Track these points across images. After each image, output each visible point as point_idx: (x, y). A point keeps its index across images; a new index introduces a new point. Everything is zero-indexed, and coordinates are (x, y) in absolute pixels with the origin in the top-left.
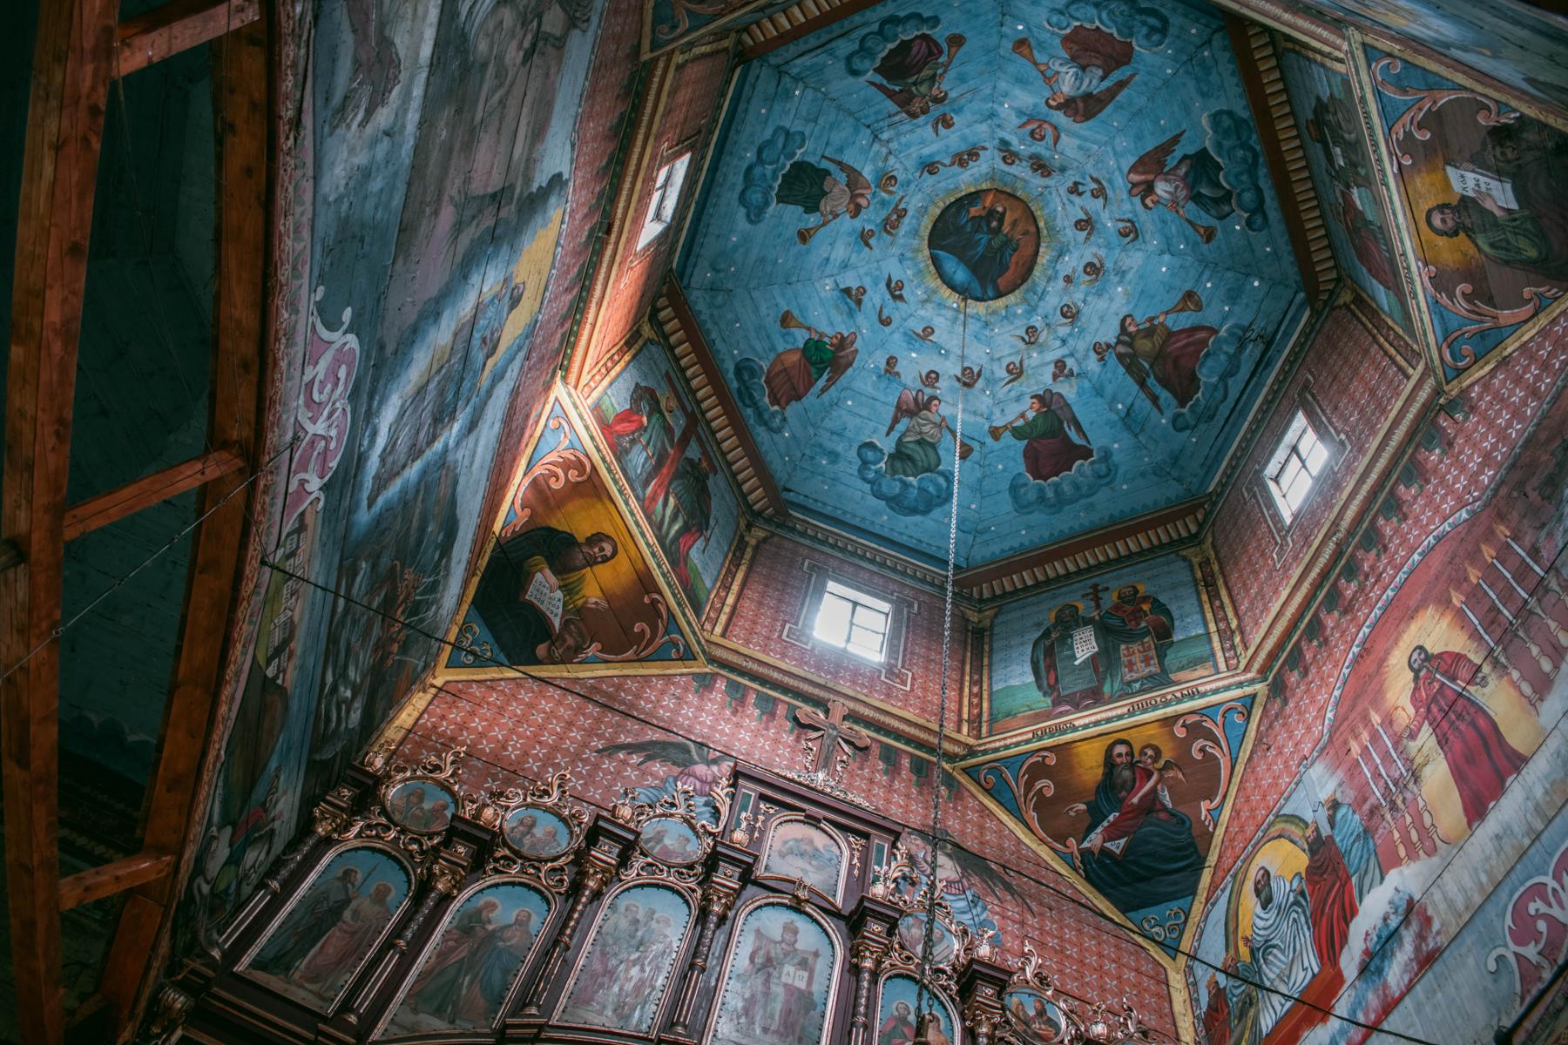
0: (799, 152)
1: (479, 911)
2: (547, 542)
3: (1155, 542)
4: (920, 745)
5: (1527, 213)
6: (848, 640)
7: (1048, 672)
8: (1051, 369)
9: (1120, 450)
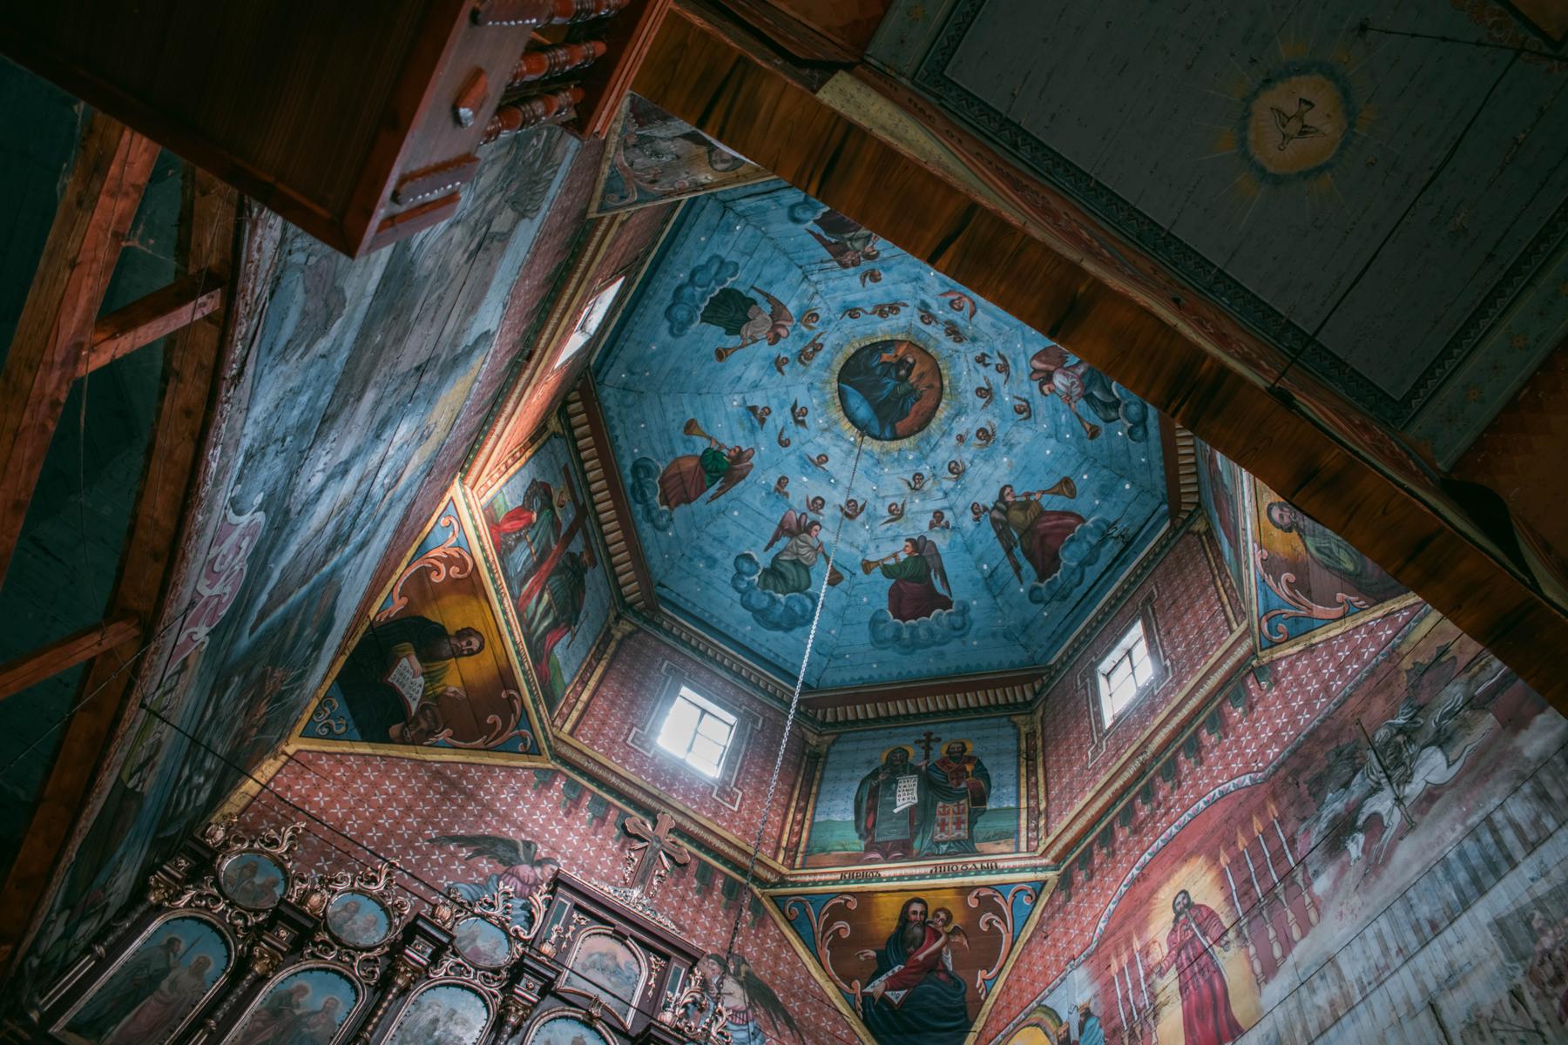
0: (730, 280)
1: (291, 994)
2: (417, 632)
3: (992, 701)
4: (736, 866)
6: (690, 749)
8: (930, 517)
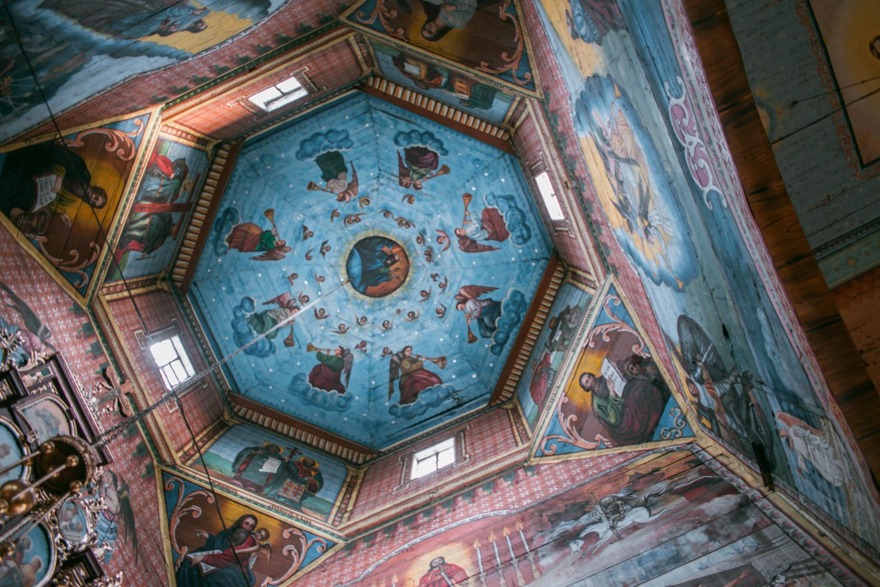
5: (623, 401)
7: (243, 463)
9: (358, 402)
